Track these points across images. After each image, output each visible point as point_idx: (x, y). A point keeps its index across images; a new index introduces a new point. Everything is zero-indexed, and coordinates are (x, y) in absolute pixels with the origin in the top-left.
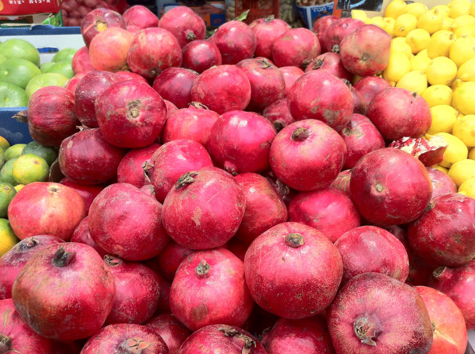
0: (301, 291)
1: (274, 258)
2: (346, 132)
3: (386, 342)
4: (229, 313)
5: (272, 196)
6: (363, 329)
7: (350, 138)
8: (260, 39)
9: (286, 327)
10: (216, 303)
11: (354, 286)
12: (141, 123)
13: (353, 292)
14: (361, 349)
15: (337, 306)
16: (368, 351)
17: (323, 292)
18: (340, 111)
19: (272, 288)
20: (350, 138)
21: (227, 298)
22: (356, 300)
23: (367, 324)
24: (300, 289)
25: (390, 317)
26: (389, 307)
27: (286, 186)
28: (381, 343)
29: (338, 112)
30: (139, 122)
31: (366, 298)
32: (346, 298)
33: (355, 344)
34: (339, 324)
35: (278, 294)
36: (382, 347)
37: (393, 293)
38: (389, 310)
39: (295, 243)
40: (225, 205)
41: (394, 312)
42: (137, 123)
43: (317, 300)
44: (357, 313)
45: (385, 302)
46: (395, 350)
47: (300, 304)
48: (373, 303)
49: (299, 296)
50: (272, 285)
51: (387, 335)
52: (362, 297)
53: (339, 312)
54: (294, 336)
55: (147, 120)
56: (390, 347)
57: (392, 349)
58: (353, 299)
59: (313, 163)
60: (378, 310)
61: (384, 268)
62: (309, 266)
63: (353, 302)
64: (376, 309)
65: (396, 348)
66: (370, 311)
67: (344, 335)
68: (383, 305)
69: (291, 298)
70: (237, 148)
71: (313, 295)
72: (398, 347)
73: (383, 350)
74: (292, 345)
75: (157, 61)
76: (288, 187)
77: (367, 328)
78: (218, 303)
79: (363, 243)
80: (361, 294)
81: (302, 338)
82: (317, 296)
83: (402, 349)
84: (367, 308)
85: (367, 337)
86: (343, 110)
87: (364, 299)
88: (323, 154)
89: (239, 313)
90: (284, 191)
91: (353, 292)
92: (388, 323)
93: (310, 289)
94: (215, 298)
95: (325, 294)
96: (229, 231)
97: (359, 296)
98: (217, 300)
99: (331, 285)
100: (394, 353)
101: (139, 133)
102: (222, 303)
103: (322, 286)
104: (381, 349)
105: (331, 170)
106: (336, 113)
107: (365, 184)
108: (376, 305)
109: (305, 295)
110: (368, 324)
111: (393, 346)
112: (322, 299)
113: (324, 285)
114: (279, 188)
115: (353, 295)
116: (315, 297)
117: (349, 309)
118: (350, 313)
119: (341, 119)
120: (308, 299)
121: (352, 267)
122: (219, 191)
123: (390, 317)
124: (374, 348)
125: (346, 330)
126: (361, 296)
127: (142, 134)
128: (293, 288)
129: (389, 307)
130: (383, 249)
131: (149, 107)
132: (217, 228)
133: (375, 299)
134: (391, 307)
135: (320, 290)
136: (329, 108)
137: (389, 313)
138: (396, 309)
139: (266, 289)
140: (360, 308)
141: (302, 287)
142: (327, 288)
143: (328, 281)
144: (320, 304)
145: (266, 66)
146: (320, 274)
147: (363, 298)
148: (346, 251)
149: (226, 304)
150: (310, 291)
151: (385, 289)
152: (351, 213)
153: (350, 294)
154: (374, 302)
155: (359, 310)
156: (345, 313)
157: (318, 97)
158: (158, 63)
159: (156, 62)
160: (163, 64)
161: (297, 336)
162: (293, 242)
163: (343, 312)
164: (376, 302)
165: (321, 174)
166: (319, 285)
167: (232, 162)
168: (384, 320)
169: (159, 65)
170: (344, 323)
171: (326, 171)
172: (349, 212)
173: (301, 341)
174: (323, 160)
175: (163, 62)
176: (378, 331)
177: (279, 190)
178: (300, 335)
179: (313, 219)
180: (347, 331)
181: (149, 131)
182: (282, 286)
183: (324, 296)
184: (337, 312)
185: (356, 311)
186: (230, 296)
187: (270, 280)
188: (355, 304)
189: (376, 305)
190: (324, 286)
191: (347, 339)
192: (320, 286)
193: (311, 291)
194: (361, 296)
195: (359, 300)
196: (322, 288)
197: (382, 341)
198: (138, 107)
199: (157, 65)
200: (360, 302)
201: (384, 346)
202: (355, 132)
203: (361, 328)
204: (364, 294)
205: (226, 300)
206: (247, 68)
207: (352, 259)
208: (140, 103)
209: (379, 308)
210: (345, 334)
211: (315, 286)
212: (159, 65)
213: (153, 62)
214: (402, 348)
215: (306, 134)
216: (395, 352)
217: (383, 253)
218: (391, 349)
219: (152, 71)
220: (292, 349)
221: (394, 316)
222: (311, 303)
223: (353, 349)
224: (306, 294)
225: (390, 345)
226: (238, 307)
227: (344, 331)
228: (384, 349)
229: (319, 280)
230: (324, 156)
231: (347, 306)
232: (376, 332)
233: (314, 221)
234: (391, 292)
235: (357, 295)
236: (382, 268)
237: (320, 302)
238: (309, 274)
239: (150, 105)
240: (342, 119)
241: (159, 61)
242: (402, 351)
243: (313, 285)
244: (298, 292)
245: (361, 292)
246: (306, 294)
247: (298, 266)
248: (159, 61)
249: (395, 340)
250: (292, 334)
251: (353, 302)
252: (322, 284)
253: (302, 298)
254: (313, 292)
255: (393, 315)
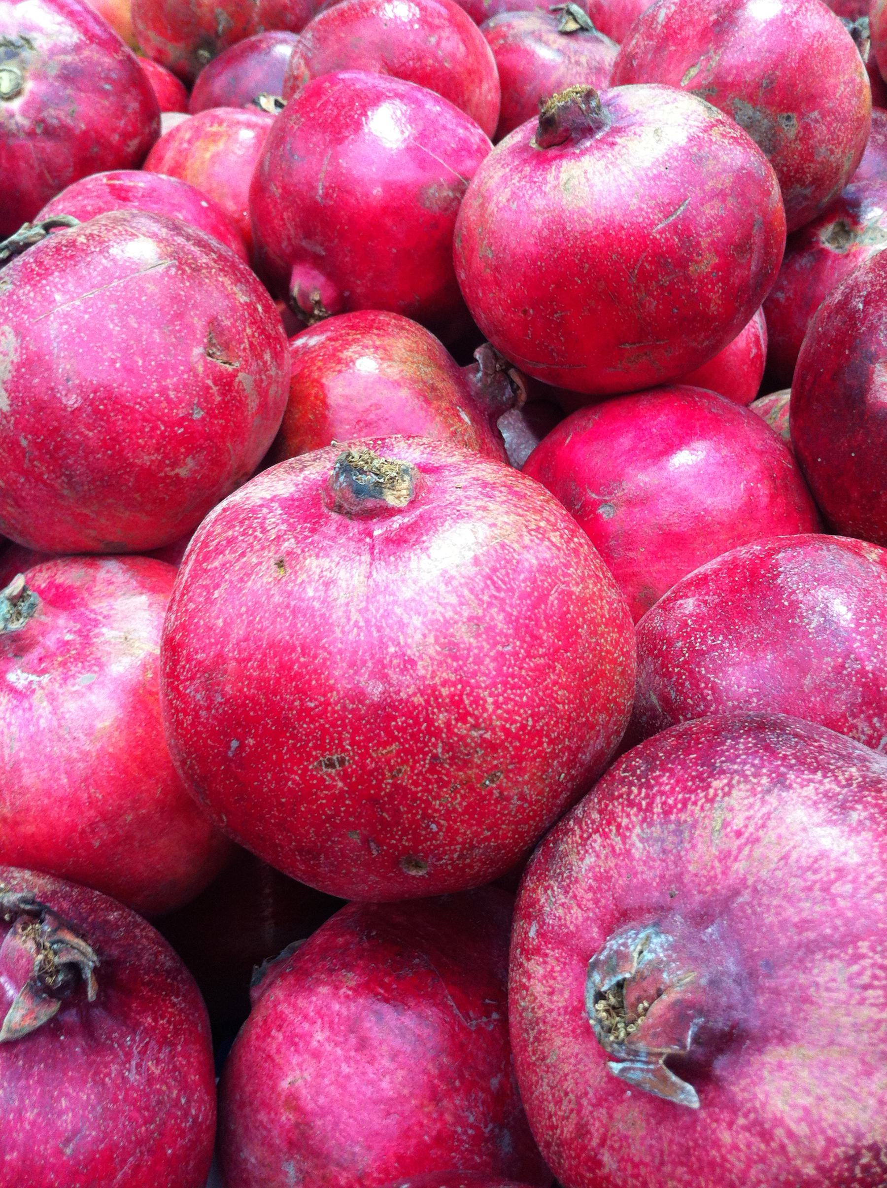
0: (341, 740)
1: (243, 554)
2: (834, 239)
3: (761, 1096)
4: (72, 828)
5: (433, 388)
6: (631, 996)
7: (847, 256)
8: (606, 8)
9: (340, 940)
10: (16, 768)
11: (651, 760)
12: (25, 123)
13: (635, 790)
14: (620, 1111)
15: (549, 855)
16: (650, 1131)
17: (466, 764)
18: (801, 115)
19: (208, 708)
20: (847, 256)
21: (75, 755)
22: (638, 830)
23: (657, 968)
24: (333, 724)
25: (811, 948)
26: (810, 889)
27: (512, 372)
28: (732, 1100)
29: (794, 121)
30: (19, 119)
31: (694, 826)
32: (595, 816)
33: (588, 1075)
34: (537, 951)
35: (235, 744)
36: (730, 1125)
37: (854, 816)
38: (809, 908)
39: (359, 491)
40: (138, 340)
41: (838, 922)
42: (13, 121)
43: (428, 804)
44: (631, 901)
45: (794, 855)
46: (810, 1158)
47: (337, 812)
48: (725, 856)
49: (331, 765)
50: (209, 688)
51: (773, 1054)
52: (673, 817)
53: (546, 889)
54: (353, 983)
55: (52, 115)
56: (779, 1132)
57: (791, 1149)
58: (625, 821)
59: (606, 233)
60: (745, 897)
61: (869, 718)
62: (398, 610)
63: (624, 838)
64: (737, 893)
65: (820, 1144)
66: (698, 898)
67: (549, 1018)
68: (779, 874)
69: (291, 772)
70: (327, 195)
71: (405, 768)
72: (831, 1142)
73: (736, 1147)
74: (331, 1028)
75: (212, 11)
76: (519, 371)
77: (652, 991)
78: (26, 771)
79: (778, 592)
80: (671, 801)
81: (387, 1001)
82: (428, 781)
83: (853, 1159)
84: (687, 879)
85: (642, 1046)
86: (815, 114)
87: (678, 832)
88: (654, 197)
89: (129, 837)
90: (503, 389)
91: (635, 790)
92: (792, 987)
93: (389, 733)
94: (16, 745)
95: (479, 778)
96: (146, 459)
97: (657, 809)
98: (22, 755)
99: (516, 737)
100: (797, 1173)
101: (22, 165)
102: (45, 774)
103: (461, 729)
104: (726, 1137)
105: (688, 280)
106: (783, 123)
107: (848, 358)
108: (740, 867)
109: (363, 766)
110: (660, 971)
111: (802, 1130)
112: (459, 803)
113: (476, 726)
114: (480, 375)
115: (631, 804)
116: (416, 783)
117: (596, 879)
118: (596, 902)
119: (808, 155)
120: (379, 787)
121: (704, 698)
122: (120, 278)
123: (811, 948)
124: (686, 1119)
125: (561, 992)
126: (667, 813)
127: (32, 167)
128: (300, 718)
129: (810, 889)
130: (872, 626)
131: (65, 66)
132: (81, 434)
133: (739, 834)
134: (826, 889)
135: (449, 747)
136: (751, 98)
137: (803, 925)
138: (855, 907)
139: (186, 714)
140: (648, 875)
141: (342, 719)
142: (491, 747)
143: (497, 705)
144: (452, 833)
145: (572, 26)
146: (455, 658)
147: (679, 823)
148: (689, 622)
149: (65, 781)
150: (385, 744)
151: (810, 790)
152: (772, 497)
153: (621, 796)
154: (729, 852)
155: (645, 886)
156: (575, 897)
157: (712, 53)
158: (216, 20)
159: (208, 15)
160: (232, 23)
161: (366, 988)
162: (350, 485)
163: (566, 892)
164: (740, 849)
165: (641, 295)
166: (441, 718)
167: (317, 262)
168: (772, 967)
169: (220, 28)
170: (557, 953)
171: (665, 281)
172: (763, 490)
173: (376, 1012)
174: (652, 224)
175: (232, 15)
176: (720, 1024)
177: (481, 380)
178: (382, 985)
179: (596, 504)
180: (567, 994)
181: (60, 161)
182: (252, 699)
183: (472, 789)
184: (540, 890)
185: (627, 889)
186: (87, 748)
187: (200, 663)
188: (628, 852)
189: (740, 867)
190: (474, 733)
191: (558, 1042)
192: (448, 724)
193: (395, 747)
194: (667, 813)
195: (656, 831)
196: (462, 738)
197: (738, 1090)
198: (22, 62)
199: (212, 26)
200: (657, 847)
201: (741, 1121)
202: (870, 234)
203: (620, 985)
204: (685, 803)
205: (69, 761)
206: (504, 29)
207: (713, 660)
208: (31, 48)
209: (755, 890)
210: (551, 1011)
211: (417, 723)
212: (220, 28)
213: (199, 12)
214: (858, 1155)
215: (593, 111)
216: (809, 1170)
217: (873, 646)
218: (783, 1147)
219: (201, 52)
220: (328, 1047)
221: (836, 945)
222: (396, 814)
223: (578, 1099)
224: (363, 757)
225: (778, 1122)
226: (127, 803)
227: (551, 993)
228: (743, 1138)
229: (445, 691)
230: (658, 205)
231: (590, 860)
232: (703, 1029)
233: (600, 511)
234: (844, 807)
235: (650, 805)
236: (855, 716)
237: (447, 817)
238: (392, 649)
239: (69, 59)
240: (812, 155)
241: (218, 10)
242: (851, 1170)
243: (409, 715)
244: (323, 739)
245: (673, 789)
246: (363, 757)
247: (342, 600)
248: (218, 10)
249: (820, 1099)
250: (350, 975)
251: (624, 838)
252: (462, 718)
253: (345, 777)
254: (407, 752)
255: (826, 938)
